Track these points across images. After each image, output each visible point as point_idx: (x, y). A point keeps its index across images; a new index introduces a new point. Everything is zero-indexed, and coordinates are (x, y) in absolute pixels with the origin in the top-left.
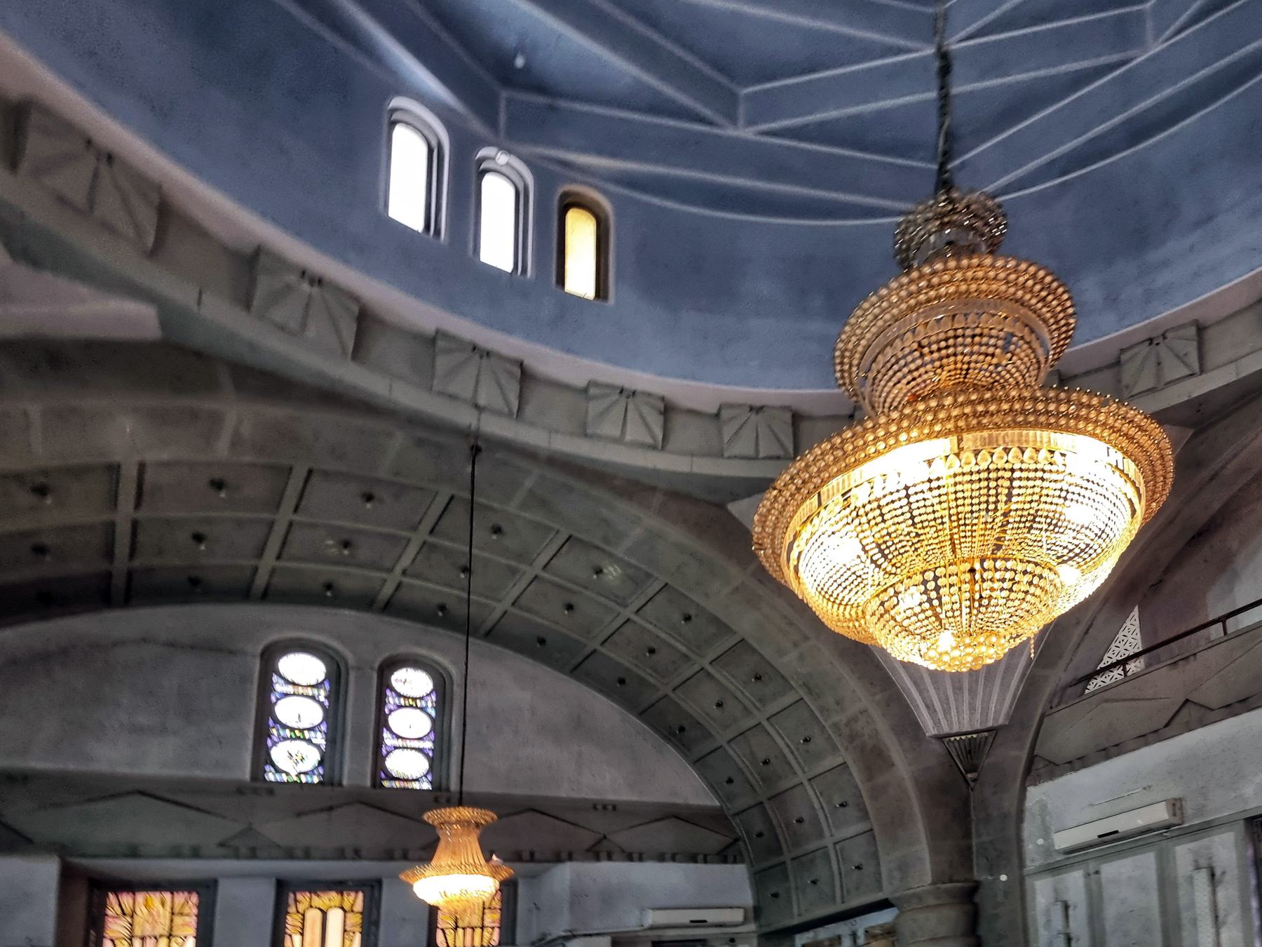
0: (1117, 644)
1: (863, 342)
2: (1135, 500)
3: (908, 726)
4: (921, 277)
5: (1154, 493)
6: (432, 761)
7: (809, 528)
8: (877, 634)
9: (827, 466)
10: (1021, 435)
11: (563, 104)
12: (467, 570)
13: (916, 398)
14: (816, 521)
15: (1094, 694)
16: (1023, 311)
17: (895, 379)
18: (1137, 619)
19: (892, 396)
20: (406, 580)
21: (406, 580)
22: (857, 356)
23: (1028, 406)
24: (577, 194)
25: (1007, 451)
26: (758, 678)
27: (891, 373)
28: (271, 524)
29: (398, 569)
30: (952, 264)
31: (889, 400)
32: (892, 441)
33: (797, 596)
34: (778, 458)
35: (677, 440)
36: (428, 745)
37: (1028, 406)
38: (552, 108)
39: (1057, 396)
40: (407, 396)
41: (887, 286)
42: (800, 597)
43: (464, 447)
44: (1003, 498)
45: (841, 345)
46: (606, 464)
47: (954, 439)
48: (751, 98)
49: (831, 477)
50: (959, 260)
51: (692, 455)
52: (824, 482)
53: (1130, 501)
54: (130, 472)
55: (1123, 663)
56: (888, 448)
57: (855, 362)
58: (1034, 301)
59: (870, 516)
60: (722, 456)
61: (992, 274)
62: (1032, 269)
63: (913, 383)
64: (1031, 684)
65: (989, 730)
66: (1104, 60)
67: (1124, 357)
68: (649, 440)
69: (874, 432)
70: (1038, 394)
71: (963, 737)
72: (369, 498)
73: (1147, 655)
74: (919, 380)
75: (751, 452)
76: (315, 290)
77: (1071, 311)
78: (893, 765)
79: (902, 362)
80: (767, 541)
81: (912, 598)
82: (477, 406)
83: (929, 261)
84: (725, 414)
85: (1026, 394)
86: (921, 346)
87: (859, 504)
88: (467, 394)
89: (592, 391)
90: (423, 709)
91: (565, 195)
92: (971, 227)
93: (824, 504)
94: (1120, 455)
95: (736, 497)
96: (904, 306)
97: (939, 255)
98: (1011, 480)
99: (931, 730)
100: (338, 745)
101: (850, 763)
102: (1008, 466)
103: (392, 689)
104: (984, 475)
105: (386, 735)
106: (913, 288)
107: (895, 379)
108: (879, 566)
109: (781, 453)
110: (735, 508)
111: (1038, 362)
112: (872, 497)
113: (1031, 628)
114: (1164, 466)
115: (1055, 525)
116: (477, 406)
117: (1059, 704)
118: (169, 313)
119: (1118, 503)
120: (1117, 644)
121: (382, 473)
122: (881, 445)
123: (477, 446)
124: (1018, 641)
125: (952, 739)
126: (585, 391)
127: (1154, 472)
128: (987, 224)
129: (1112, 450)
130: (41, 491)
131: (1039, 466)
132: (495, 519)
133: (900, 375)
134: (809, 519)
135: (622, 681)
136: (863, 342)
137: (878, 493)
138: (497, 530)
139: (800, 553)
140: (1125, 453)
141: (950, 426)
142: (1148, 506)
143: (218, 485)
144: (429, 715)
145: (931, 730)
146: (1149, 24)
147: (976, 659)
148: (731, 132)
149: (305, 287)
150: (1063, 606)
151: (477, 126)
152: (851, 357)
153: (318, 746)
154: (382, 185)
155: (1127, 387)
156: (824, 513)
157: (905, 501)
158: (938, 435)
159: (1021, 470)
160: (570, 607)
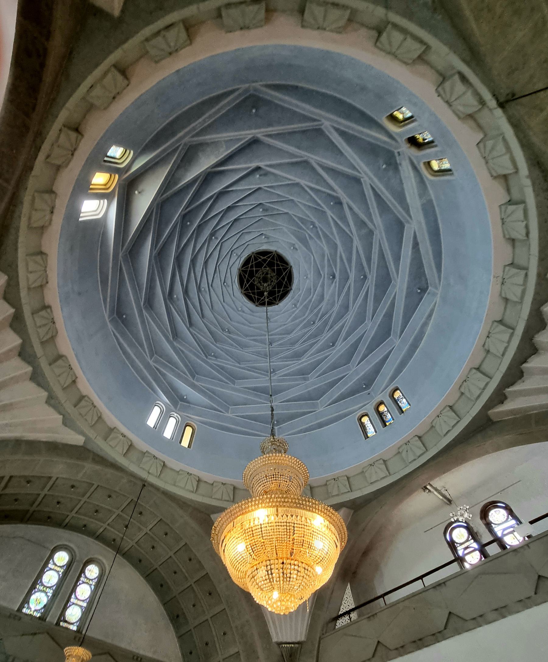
0: (344, 602)
1: (251, 472)
2: (336, 541)
3: (265, 634)
4: (266, 457)
5: (342, 539)
6: (83, 613)
7: (229, 534)
8: (249, 587)
9: (237, 512)
10: (295, 511)
11: (191, 405)
12: (127, 527)
13: (266, 493)
14: (232, 532)
15: (340, 629)
16: (294, 470)
17: (259, 485)
18: (350, 588)
19: (258, 490)
20: (108, 527)
21: (108, 527)
22: (249, 476)
23: (297, 501)
24: (190, 423)
25: (292, 516)
26: (210, 594)
27: (258, 483)
28: (80, 500)
29: (107, 523)
30: (274, 455)
31: (257, 491)
32: (256, 506)
33: (223, 563)
34: (228, 501)
35: (200, 491)
36: (85, 605)
37: (297, 501)
38: (189, 406)
39: (305, 499)
40: (133, 468)
41: (257, 458)
42: (224, 563)
43: (140, 484)
44: (292, 534)
45: (244, 472)
46: (179, 495)
47: (275, 508)
48: (231, 408)
49: (238, 516)
50: (276, 454)
51: (203, 496)
52: (236, 518)
53: (335, 541)
54: (54, 479)
55: (348, 613)
56: (256, 509)
57: (248, 478)
58: (297, 467)
59: (249, 533)
60: (211, 497)
61: (285, 459)
62: (295, 459)
63: (264, 487)
64: (314, 617)
65: (298, 643)
66: (311, 410)
67: (328, 483)
68: (192, 489)
69: (251, 503)
70: (300, 498)
71: (288, 645)
72: (110, 496)
73: (358, 610)
74: (266, 486)
75: (220, 498)
76: (123, 438)
77: (307, 471)
78: (258, 658)
79: (261, 480)
80: (216, 537)
81: (262, 572)
82: (149, 473)
83: (268, 453)
84: (214, 484)
85: (296, 497)
86: (266, 476)
87: (246, 528)
88: (147, 469)
89: (180, 472)
90: (91, 585)
91: (188, 423)
92: (279, 445)
93: (235, 526)
94: (328, 522)
95: (214, 513)
96: (262, 464)
97: (271, 451)
98: (294, 527)
99: (275, 639)
100: (55, 597)
101: (241, 652)
102: (293, 522)
103: (85, 574)
104: (285, 524)
105: (73, 596)
106: (264, 459)
107: (259, 485)
108: (251, 555)
109: (229, 499)
110: (213, 516)
111: (300, 486)
112: (250, 527)
113: (307, 595)
114: (343, 529)
115: (310, 546)
116: (149, 473)
117: (326, 633)
118: (88, 439)
119: (331, 541)
120: (344, 602)
121: (117, 489)
122: (253, 508)
123: (145, 484)
124: (302, 601)
125: (283, 645)
126: (178, 472)
127: (340, 531)
128: (283, 445)
129: (326, 521)
130: (28, 482)
131: (303, 523)
132: (141, 510)
133: (260, 484)
134: (230, 531)
135: (162, 586)
136: (251, 472)
137: (252, 525)
138: (141, 513)
139: (226, 545)
140: (330, 522)
141: (274, 504)
142: (341, 545)
143: (73, 487)
144: (91, 588)
145: (275, 639)
146: (319, 405)
147: (287, 608)
148: (226, 414)
149: (121, 437)
150: (319, 585)
151: (172, 408)
152: (247, 476)
153: (48, 596)
154: (148, 416)
155: (330, 493)
156: (235, 530)
157: (260, 530)
158: (271, 507)
159: (297, 524)
160: (153, 547)
